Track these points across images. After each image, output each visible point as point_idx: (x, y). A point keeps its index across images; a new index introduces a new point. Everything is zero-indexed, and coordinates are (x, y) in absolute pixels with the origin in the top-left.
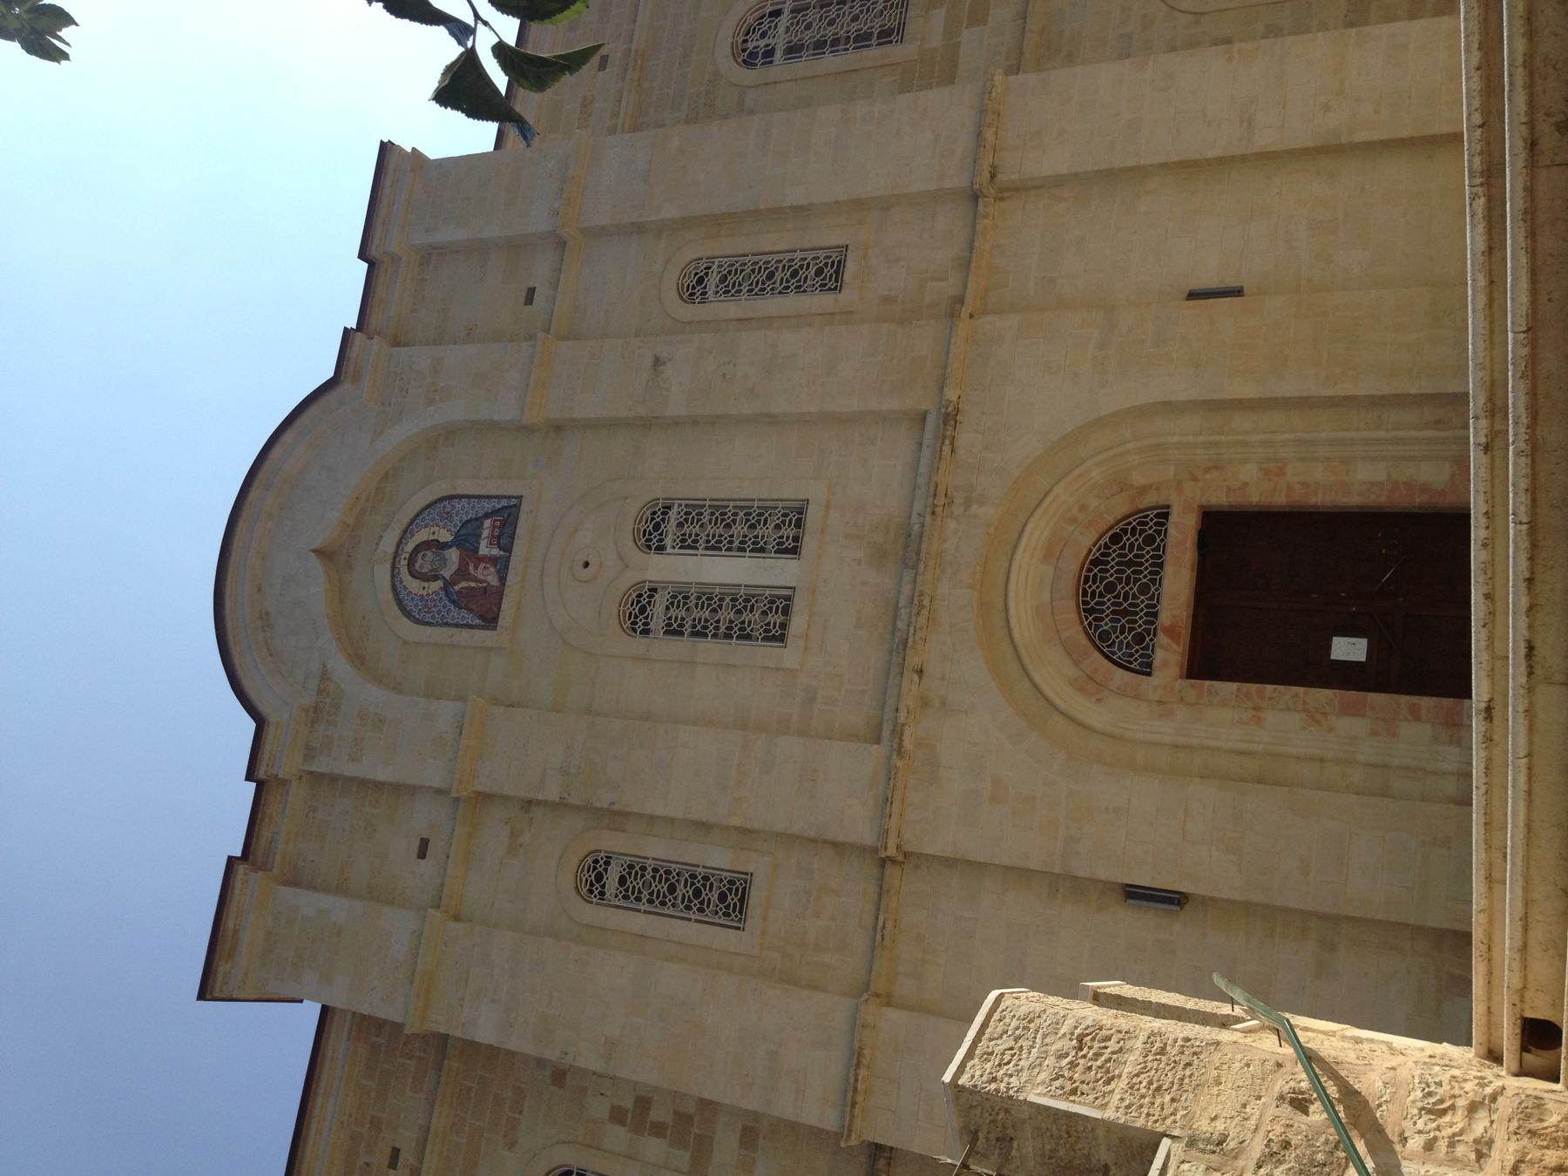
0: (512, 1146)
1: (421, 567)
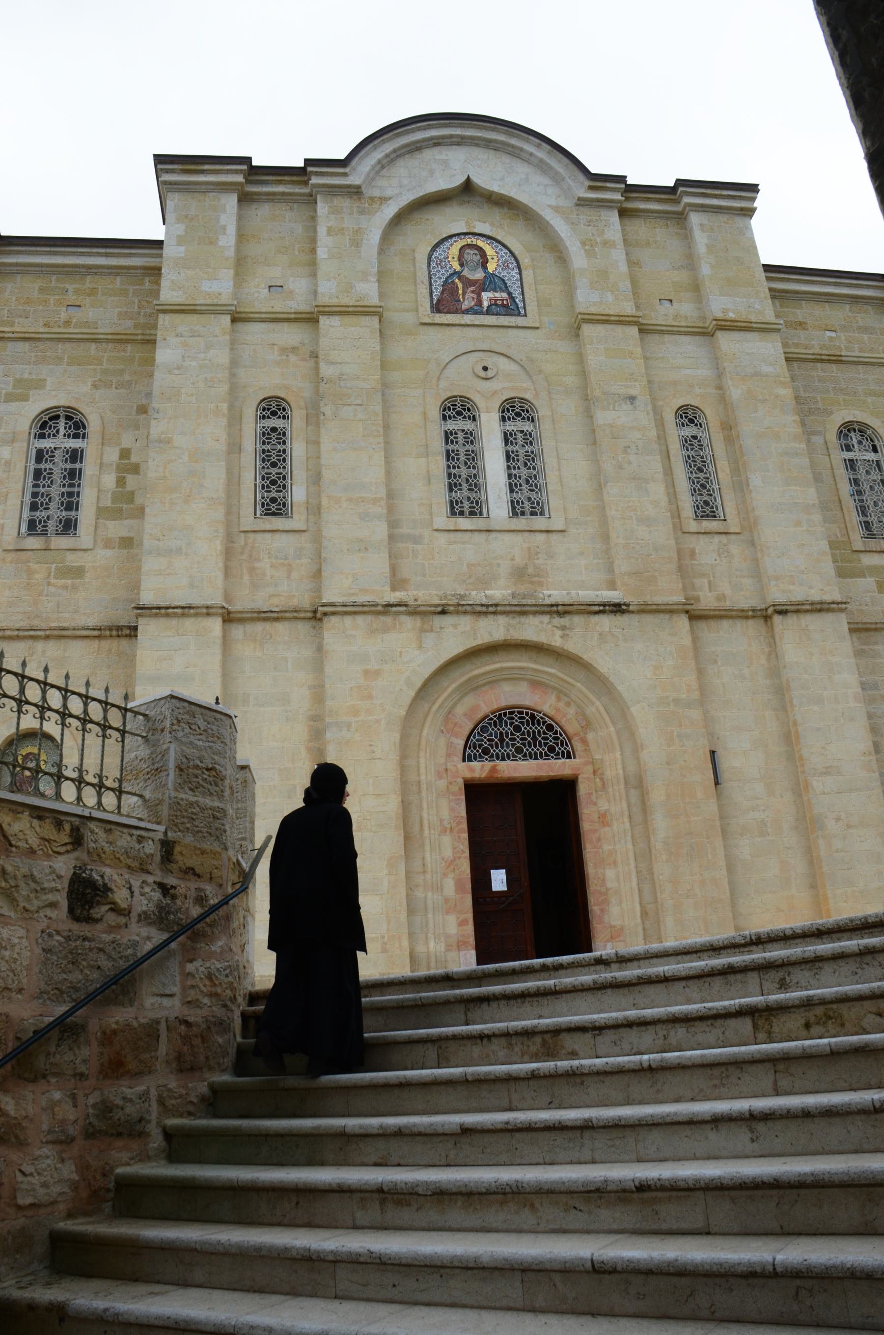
0: (95, 386)
1: (468, 254)
